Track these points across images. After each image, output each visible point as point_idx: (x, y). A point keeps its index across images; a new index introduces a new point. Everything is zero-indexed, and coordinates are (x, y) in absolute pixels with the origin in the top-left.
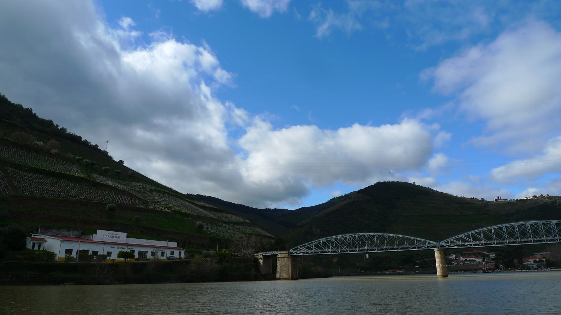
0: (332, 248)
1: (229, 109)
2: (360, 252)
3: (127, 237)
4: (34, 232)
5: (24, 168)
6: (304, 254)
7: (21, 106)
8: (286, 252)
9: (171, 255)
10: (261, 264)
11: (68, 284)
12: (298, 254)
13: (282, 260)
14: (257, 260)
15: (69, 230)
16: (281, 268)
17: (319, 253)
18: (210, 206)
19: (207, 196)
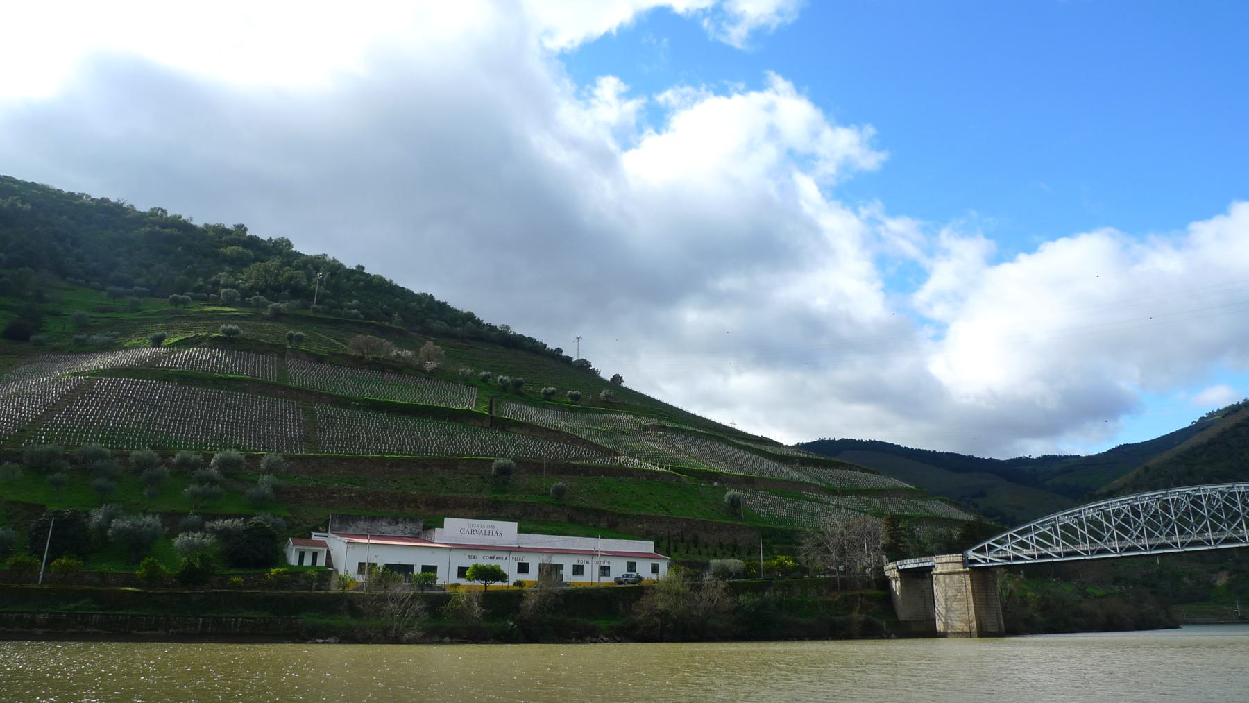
0: (1092, 542)
1: (872, 221)
2: (1188, 549)
3: (520, 531)
4: (321, 529)
5: (353, 403)
6: (1009, 563)
7: (431, 297)
8: (955, 559)
9: (628, 573)
10: (898, 593)
11: (322, 641)
12: (991, 561)
13: (947, 581)
14: (885, 583)
15: (395, 520)
16: (946, 605)
17: (1054, 558)
18: (802, 455)
19: (864, 441)
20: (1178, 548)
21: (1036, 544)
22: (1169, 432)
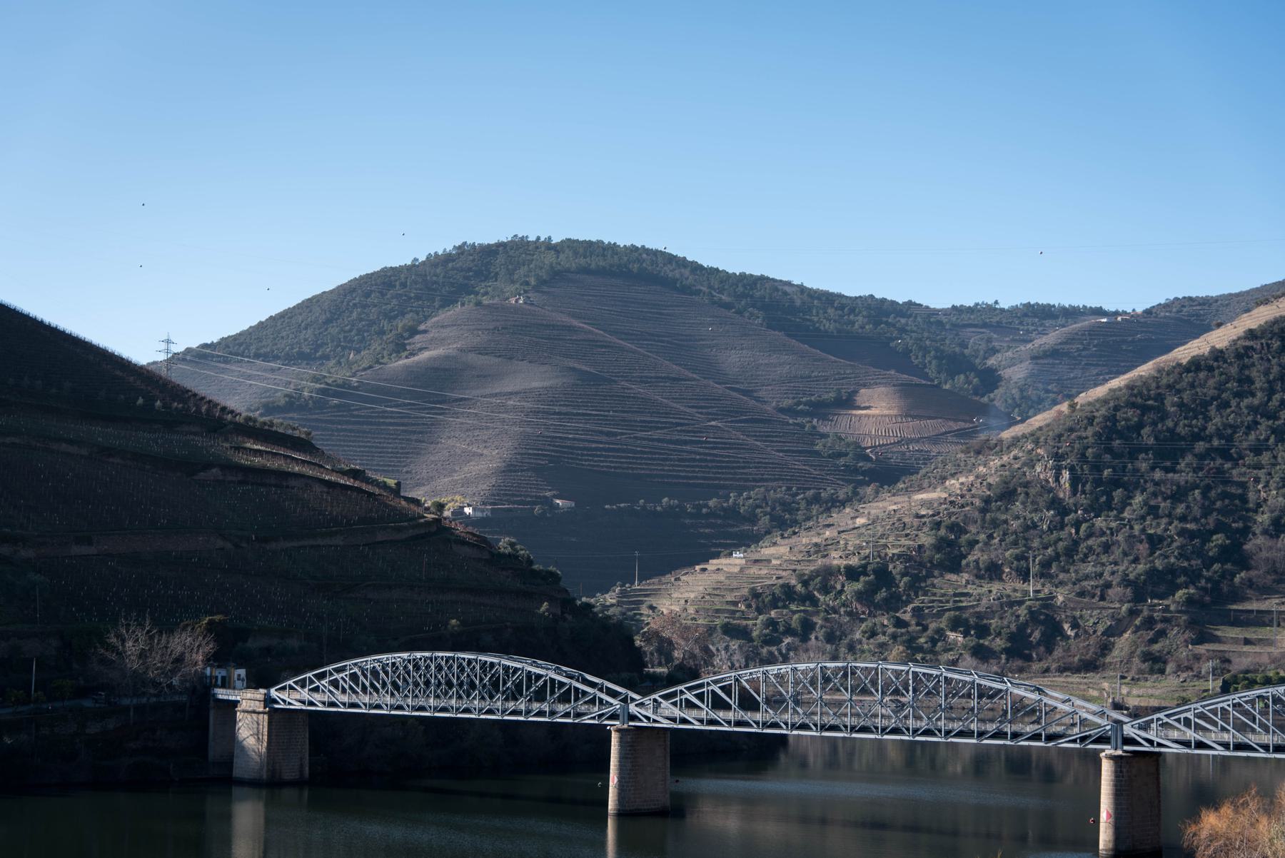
20: (817, 731)
21: (1217, 723)
22: (377, 267)
